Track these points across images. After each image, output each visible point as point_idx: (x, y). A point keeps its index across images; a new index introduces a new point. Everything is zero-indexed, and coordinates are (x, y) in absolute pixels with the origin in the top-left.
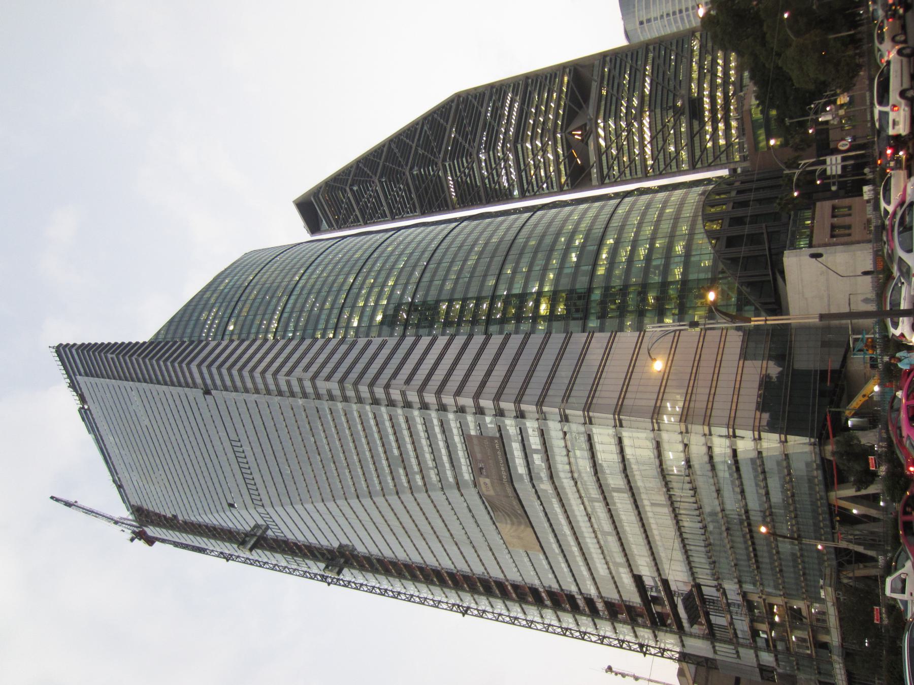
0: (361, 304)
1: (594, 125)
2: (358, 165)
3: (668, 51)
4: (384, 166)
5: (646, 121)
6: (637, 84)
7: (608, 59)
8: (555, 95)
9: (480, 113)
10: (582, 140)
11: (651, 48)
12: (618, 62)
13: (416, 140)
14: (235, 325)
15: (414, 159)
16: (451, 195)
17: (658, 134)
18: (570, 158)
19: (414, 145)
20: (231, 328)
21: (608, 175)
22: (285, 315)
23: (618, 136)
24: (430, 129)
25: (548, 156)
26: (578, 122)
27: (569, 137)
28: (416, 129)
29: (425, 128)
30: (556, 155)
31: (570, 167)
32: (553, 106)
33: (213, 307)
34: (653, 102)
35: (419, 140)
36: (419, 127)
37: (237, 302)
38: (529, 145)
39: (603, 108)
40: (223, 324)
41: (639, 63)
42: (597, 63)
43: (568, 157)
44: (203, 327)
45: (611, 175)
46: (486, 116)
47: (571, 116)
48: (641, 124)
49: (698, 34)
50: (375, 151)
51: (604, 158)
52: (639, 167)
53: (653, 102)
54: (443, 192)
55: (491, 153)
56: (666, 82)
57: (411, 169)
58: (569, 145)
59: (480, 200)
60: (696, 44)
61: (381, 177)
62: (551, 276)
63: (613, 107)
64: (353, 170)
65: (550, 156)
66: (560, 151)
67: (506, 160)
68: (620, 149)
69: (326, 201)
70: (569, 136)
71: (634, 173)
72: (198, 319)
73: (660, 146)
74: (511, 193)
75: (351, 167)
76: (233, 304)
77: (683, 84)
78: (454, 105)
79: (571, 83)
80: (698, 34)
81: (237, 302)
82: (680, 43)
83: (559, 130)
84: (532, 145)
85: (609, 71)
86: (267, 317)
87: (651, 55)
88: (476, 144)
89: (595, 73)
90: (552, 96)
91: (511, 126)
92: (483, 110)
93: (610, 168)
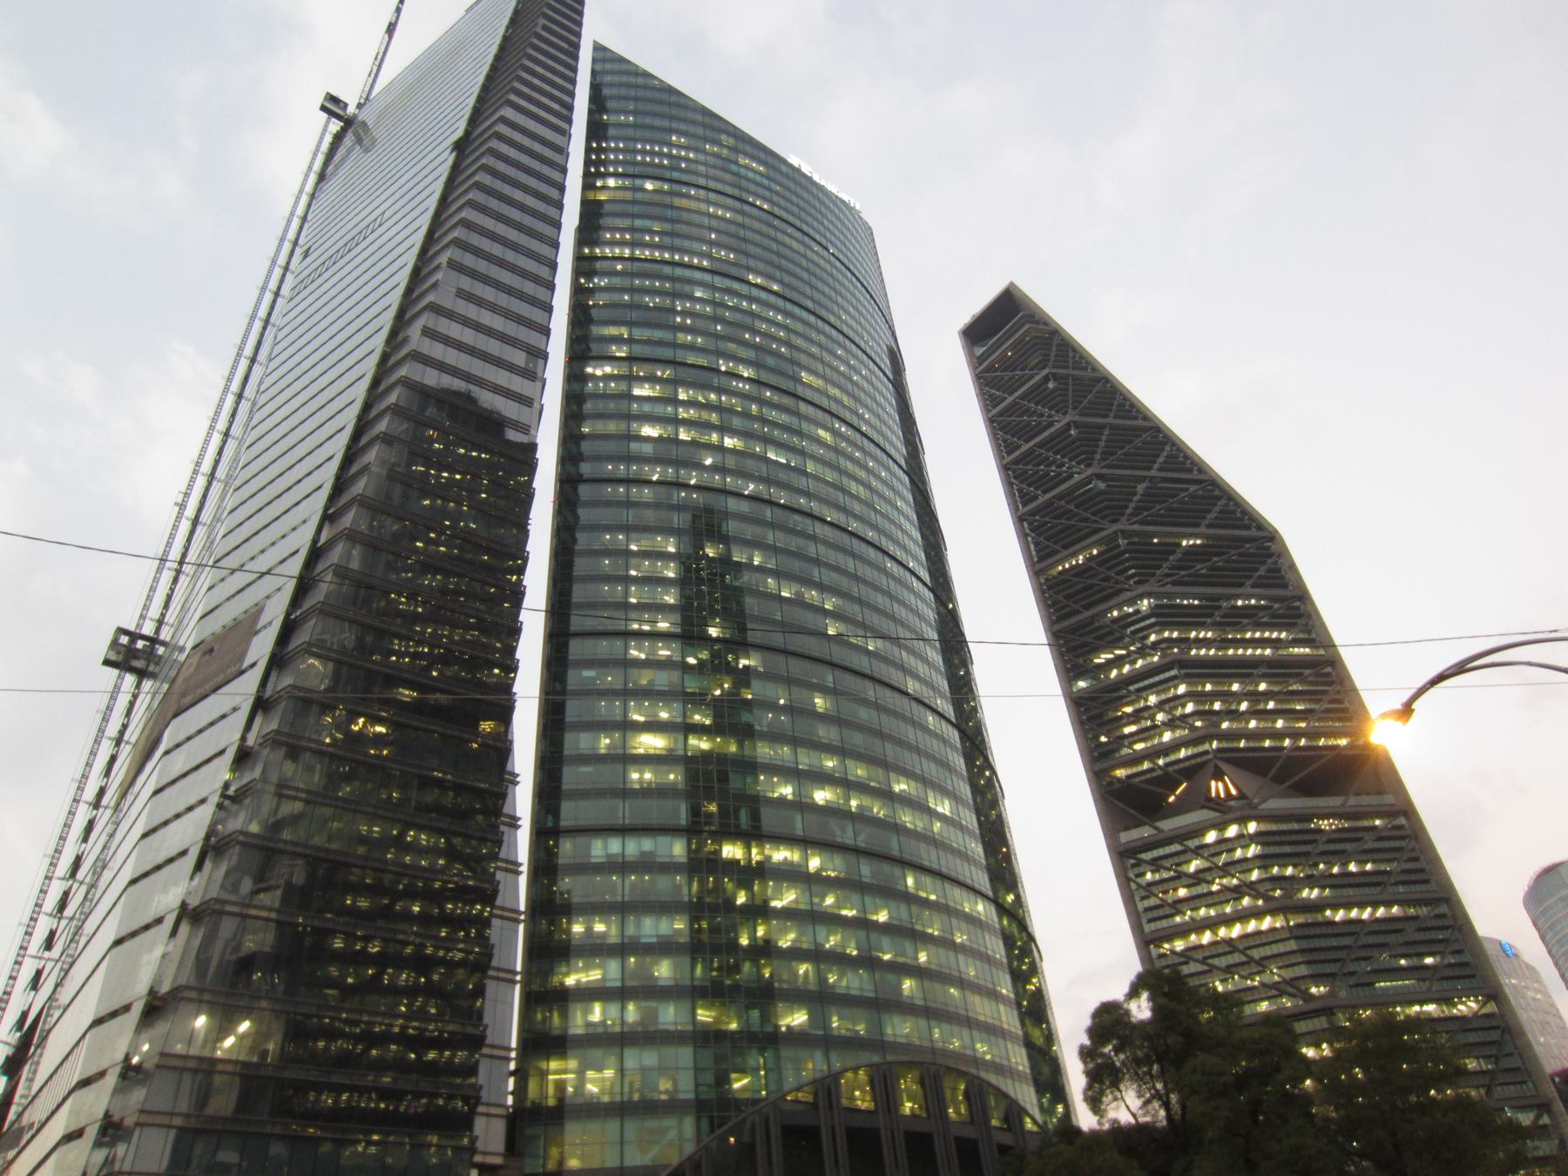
0: (682, 396)
1: (1238, 814)
2: (1098, 380)
3: (1440, 947)
4: (1103, 427)
5: (1267, 923)
6: (1350, 891)
7: (1402, 821)
8: (1303, 725)
9: (1241, 585)
10: (1209, 799)
11: (1443, 909)
12: (1397, 844)
13: (1163, 474)
14: (655, 191)
15: (1120, 478)
16: (1061, 561)
17: (1243, 952)
18: (1167, 780)
19: (1153, 473)
20: (649, 186)
21: (1139, 863)
22: (667, 270)
23: (1226, 870)
24: (1193, 496)
25: (1160, 728)
26: (1252, 784)
27: (1210, 769)
28: (1190, 471)
29: (1193, 488)
30: (1175, 746)
31: (1147, 781)
32: (1283, 731)
33: (696, 150)
34: (1313, 931)
35: (1165, 480)
36: (1195, 475)
37: (801, 230)
38: (1182, 689)
39: (1284, 827)
40: (649, 171)
41: (1401, 889)
42: (1389, 799)
43: (1166, 774)
44: (652, 142)
45: (1141, 869)
46: (1238, 597)
47: (1254, 764)
48: (1258, 914)
49: (1491, 1008)
50: (1132, 406)
51: (1176, 847)
52: (1164, 923)
53: (1313, 931)
54: (1065, 547)
55: (1153, 620)
56: (1364, 953)
57: (1100, 477)
58: (1194, 771)
59: (1059, 619)
60: (1467, 1007)
61: (1077, 425)
62: (830, 764)
63: (1288, 849)
64: (1089, 373)
65: (1167, 736)
66: (1183, 753)
67: (1142, 652)
68: (1198, 878)
69: (1021, 339)
70: (1210, 769)
71: (1150, 915)
72: (672, 131)
73: (1216, 962)
74: (1079, 676)
75: (1094, 369)
76: (797, 223)
77: (1363, 992)
78: (1253, 533)
79: (1331, 754)
80: (1491, 1008)
81: (801, 230)
82: (1464, 972)
83: (1225, 745)
84: (1183, 696)
85: (1375, 828)
86: (667, 240)
87: (1423, 911)
88: (1169, 588)
89: (1365, 800)
90: (1302, 720)
91: (1218, 649)
92: (1247, 589)
93: (1156, 865)
